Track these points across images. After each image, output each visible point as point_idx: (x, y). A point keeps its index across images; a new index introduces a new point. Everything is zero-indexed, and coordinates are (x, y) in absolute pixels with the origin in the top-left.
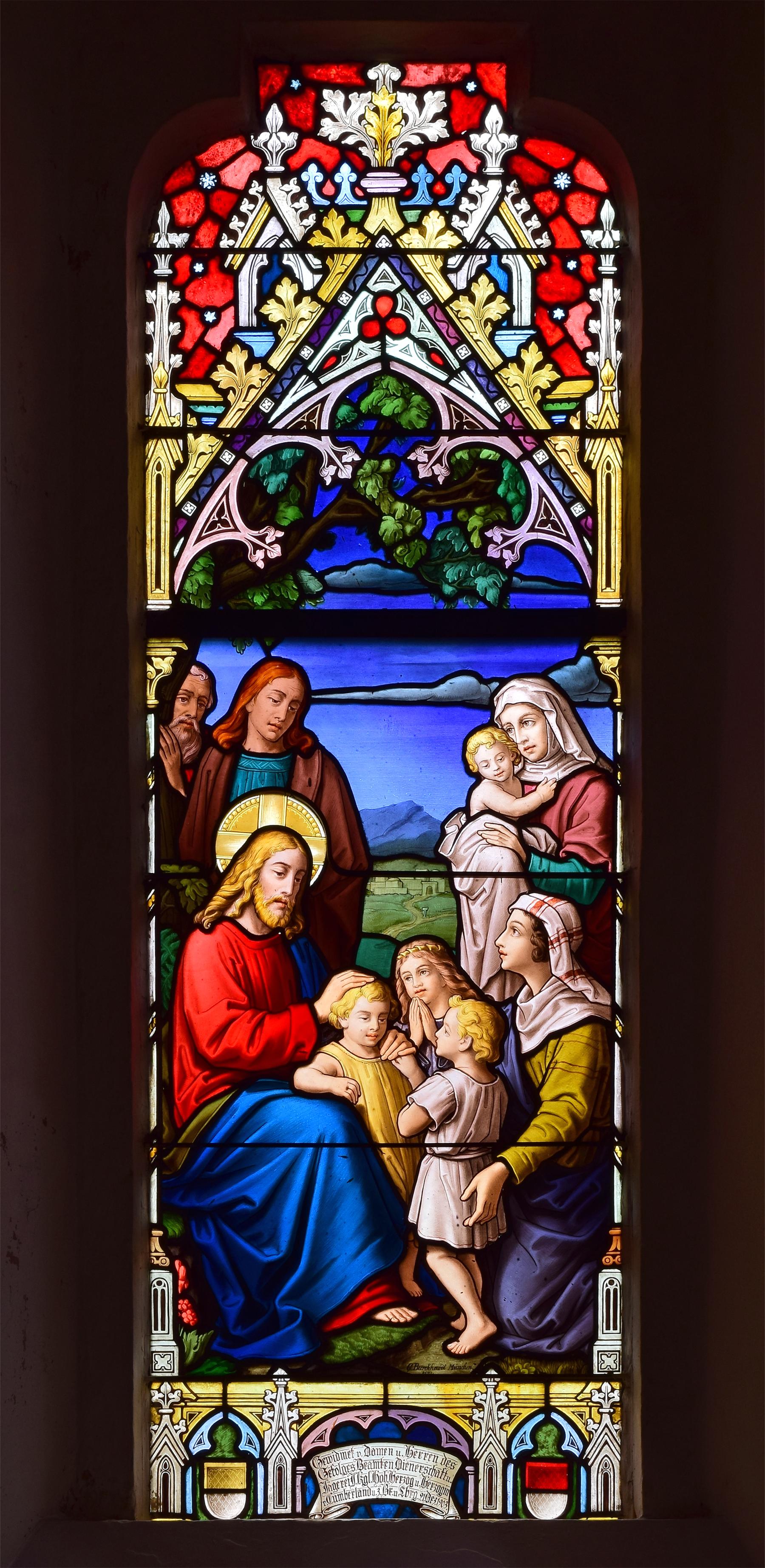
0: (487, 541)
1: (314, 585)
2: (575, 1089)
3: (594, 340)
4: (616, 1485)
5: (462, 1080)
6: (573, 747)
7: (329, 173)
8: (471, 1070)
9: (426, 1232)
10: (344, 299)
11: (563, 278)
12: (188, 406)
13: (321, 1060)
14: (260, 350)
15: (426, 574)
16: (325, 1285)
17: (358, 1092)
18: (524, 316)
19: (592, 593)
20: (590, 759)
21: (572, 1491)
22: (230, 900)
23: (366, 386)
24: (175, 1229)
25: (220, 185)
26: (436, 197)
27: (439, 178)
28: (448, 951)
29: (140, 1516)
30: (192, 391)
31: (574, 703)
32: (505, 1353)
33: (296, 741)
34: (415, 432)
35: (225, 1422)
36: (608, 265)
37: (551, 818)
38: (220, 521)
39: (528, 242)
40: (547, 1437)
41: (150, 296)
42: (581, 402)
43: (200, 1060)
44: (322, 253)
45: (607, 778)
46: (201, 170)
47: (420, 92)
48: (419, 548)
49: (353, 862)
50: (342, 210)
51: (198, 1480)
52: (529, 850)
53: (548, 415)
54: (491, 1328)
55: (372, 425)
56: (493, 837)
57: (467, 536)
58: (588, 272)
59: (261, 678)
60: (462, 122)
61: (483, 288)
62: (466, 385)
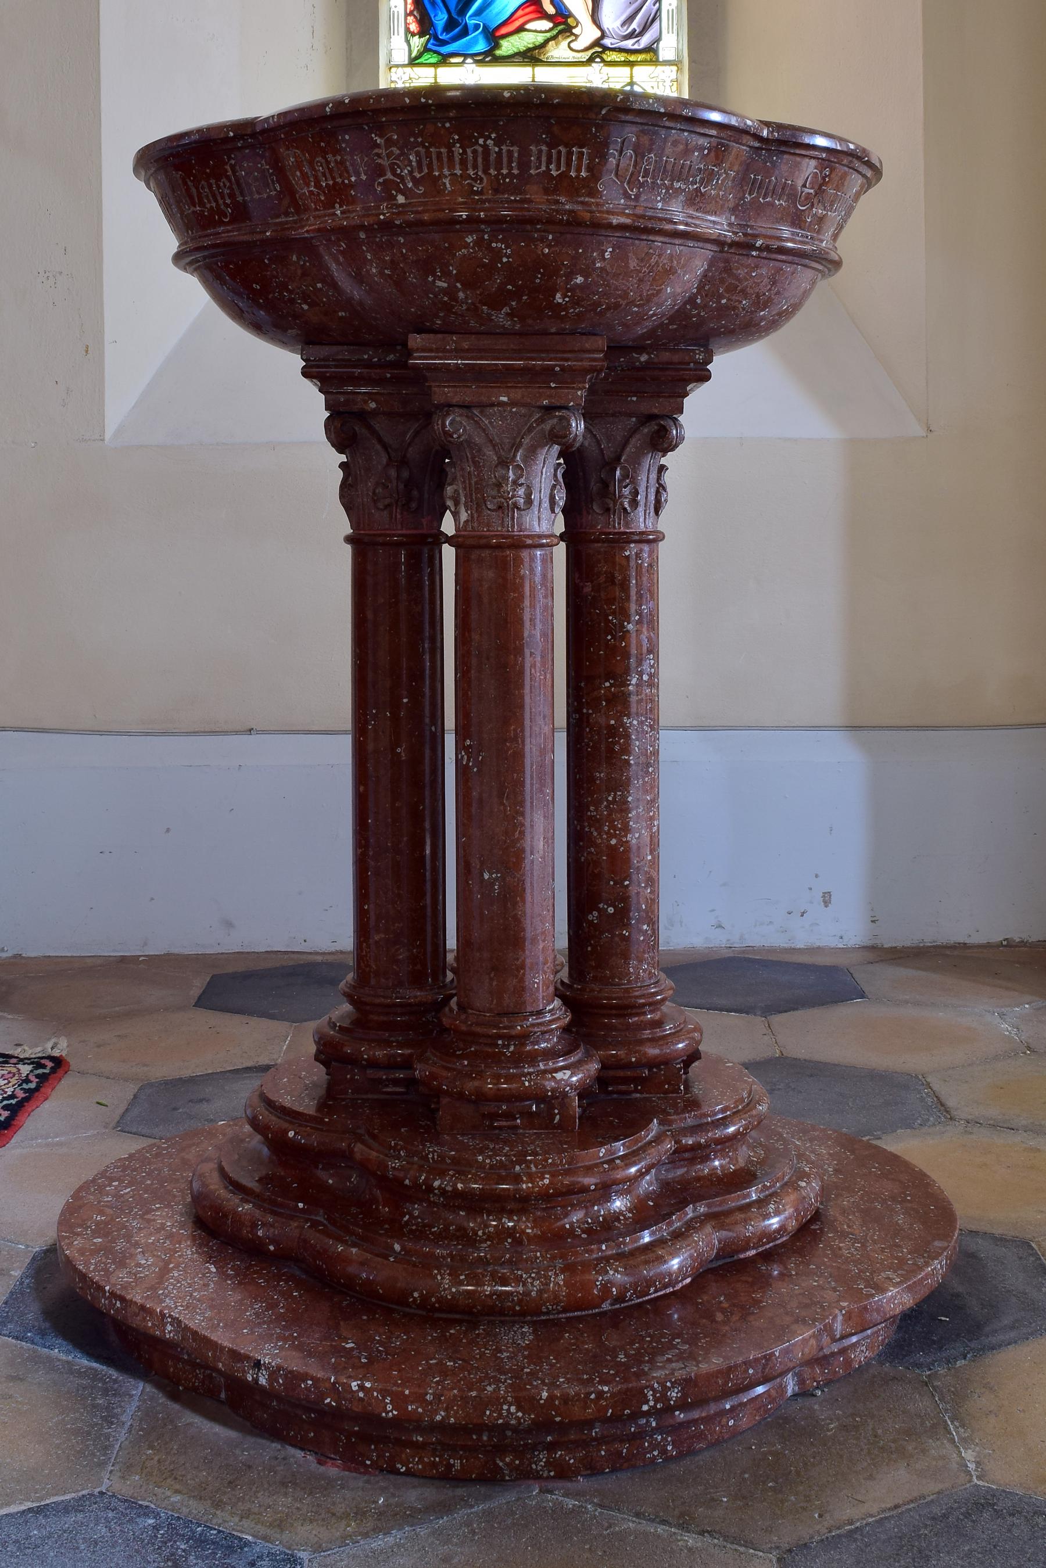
32: (606, 49)
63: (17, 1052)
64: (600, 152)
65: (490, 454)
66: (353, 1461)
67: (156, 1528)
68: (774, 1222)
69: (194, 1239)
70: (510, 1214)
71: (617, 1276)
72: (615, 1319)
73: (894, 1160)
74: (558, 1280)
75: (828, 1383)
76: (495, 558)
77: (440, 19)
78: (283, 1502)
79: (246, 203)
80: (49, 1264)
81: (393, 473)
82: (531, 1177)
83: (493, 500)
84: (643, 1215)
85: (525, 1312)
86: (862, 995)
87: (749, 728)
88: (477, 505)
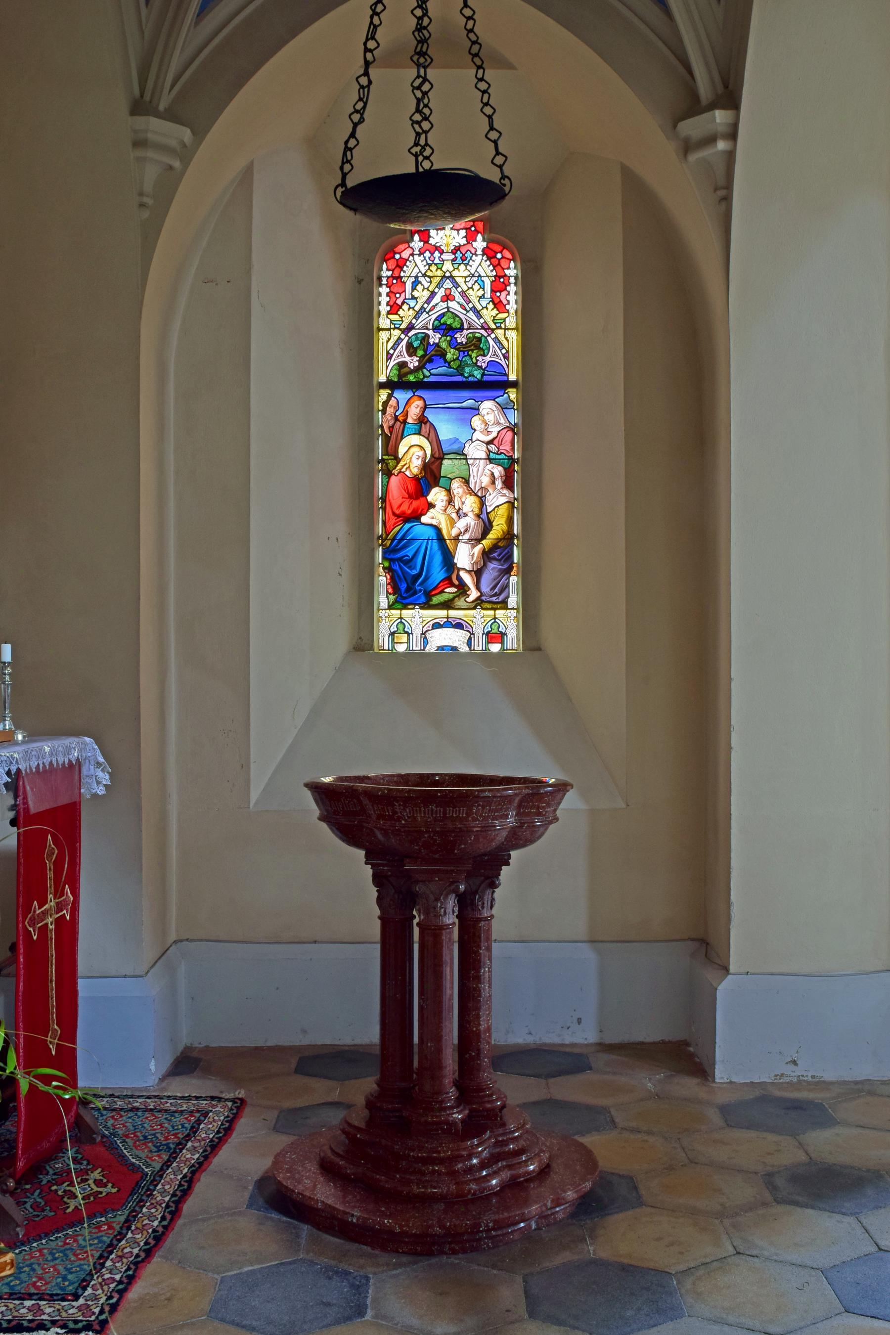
0: (477, 361)
1: (427, 374)
2: (503, 522)
3: (508, 301)
4: (515, 641)
5: (470, 520)
6: (502, 421)
7: (432, 254)
8: (473, 517)
9: (459, 565)
10: (436, 290)
11: (499, 284)
12: (391, 321)
13: (429, 514)
14: (412, 305)
15: (460, 370)
16: (430, 581)
17: (440, 523)
18: (488, 295)
19: (507, 376)
20: (508, 425)
21: (502, 642)
22: (403, 466)
23: (443, 315)
24: (386, 564)
25: (401, 258)
26: (463, 260)
27: (464, 255)
28: (467, 482)
29: (376, 650)
30: (392, 317)
31: (503, 408)
32: (483, 601)
33: (422, 420)
34: (457, 329)
35: (401, 622)
36: (512, 280)
37: (496, 442)
38: (400, 355)
39: (489, 274)
40: (495, 627)
41: (381, 289)
42: (505, 319)
43: (394, 514)
44: (430, 277)
45: (513, 430)
46: (395, 253)
47: (458, 230)
48: (458, 363)
49: (438, 457)
50: (436, 264)
51: (393, 639)
52: (490, 451)
53: (495, 324)
54: (479, 594)
55: (444, 327)
56: (479, 448)
57: (472, 359)
58: (506, 282)
59: (412, 401)
60: (470, 238)
61: (476, 287)
62: (471, 314)
63: (223, 1096)
64: (470, 809)
65: (431, 896)
66: (384, 1249)
67: (321, 1268)
68: (532, 1168)
69: (321, 1173)
70: (437, 1165)
71: (473, 1186)
72: (472, 1201)
73: (582, 1144)
74: (453, 1187)
75: (547, 1225)
76: (433, 934)
77: (404, 586)
78: (362, 1261)
79: (348, 808)
80: (262, 1183)
81: (396, 896)
82: (444, 1152)
83: (431, 911)
84: (483, 1165)
85: (442, 1198)
86: (590, 1069)
87: (544, 941)
88: (427, 914)
